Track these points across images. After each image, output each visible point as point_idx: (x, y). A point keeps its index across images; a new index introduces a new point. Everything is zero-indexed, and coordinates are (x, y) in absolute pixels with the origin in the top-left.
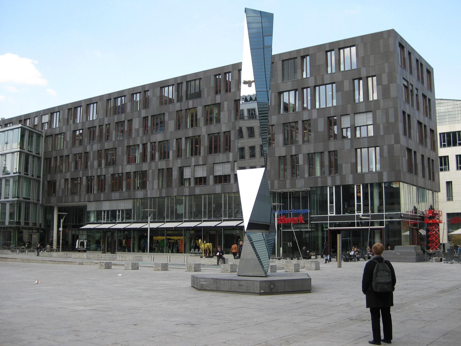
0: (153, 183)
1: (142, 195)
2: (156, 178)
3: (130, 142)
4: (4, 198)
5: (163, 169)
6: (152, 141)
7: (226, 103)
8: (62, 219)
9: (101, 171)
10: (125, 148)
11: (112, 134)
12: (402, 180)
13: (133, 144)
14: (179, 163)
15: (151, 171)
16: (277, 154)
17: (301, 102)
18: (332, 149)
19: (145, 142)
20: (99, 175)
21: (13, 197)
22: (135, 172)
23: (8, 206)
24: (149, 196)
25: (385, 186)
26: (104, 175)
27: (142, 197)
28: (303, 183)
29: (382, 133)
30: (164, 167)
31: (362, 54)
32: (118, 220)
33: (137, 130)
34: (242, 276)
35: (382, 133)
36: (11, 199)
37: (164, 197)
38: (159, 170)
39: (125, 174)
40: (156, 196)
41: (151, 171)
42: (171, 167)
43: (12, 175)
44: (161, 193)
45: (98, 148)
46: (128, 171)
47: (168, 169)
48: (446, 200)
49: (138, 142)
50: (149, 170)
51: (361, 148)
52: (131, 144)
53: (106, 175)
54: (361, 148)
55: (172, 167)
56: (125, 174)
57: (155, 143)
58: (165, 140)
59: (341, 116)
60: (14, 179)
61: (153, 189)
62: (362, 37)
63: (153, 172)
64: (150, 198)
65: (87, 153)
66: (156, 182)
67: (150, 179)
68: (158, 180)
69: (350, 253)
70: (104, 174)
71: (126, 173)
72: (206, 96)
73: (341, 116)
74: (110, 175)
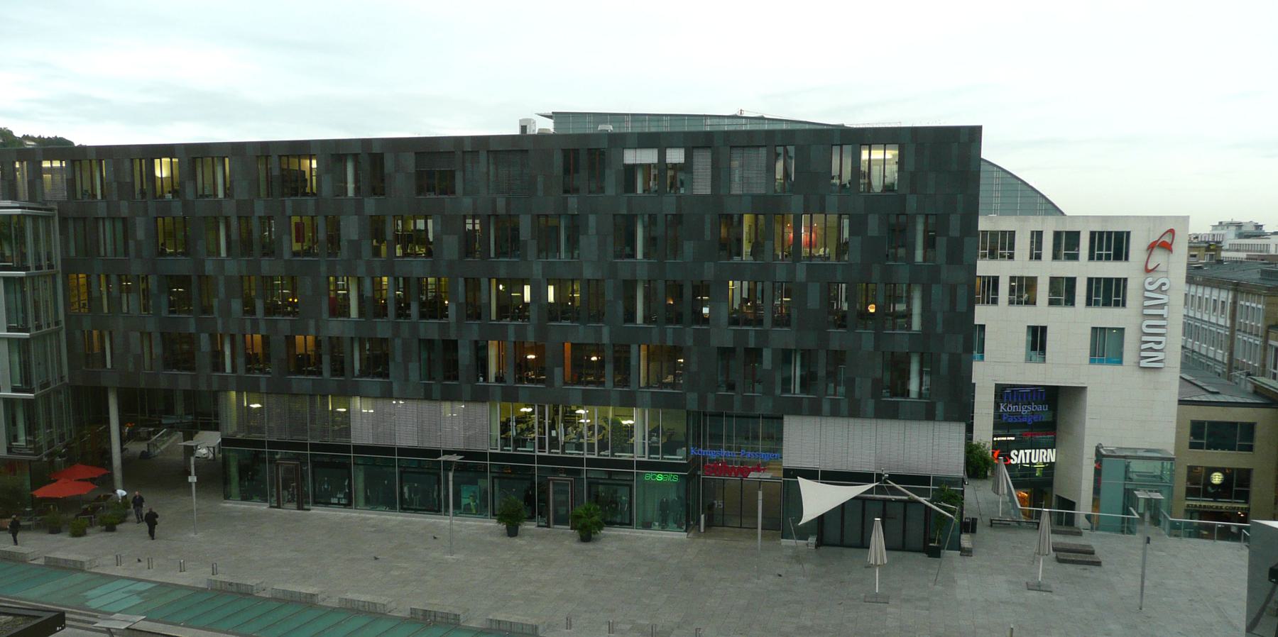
0: (406, 369)
7: (592, 219)
14: (474, 330)
15: (398, 342)
16: (715, 342)
18: (835, 345)
25: (804, 399)
28: (770, 405)
29: (939, 329)
30: (436, 337)
31: (910, 165)
33: (355, 246)
35: (939, 329)
41: (398, 342)
42: (453, 337)
48: (1088, 362)
53: (271, 338)
55: (456, 338)
59: (693, 147)
62: (915, 131)
65: (203, 278)
66: (414, 367)
67: (399, 358)
69: (1012, 461)
72: (540, 193)
73: (693, 147)
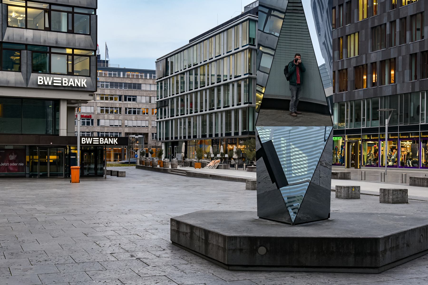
1: (391, 91)
2: (408, 67)
3: (375, 22)
4: (237, 104)
5: (416, 54)
6: (402, 16)
8: (387, 118)
9: (343, 65)
10: (369, 30)
11: (354, 12)
12: (95, 136)
13: (379, 24)
15: (400, 58)
17: (57, 117)
19: (392, 19)
20: (340, 69)
21: (245, 104)
22: (381, 62)
23: (240, 112)
24: (398, 92)
26: (346, 69)
27: (390, 94)
30: (418, 51)
32: (363, 126)
34: (372, 195)
36: (243, 105)
37: (418, 92)
38: (411, 55)
39: (369, 65)
40: (407, 92)
41: (400, 58)
43: (243, 77)
44: (413, 87)
45: (338, 35)
46: (373, 60)
47: (422, 53)
49: (384, 19)
50: (398, 57)
51: (47, 134)
52: (376, 24)
54: (47, 134)
56: (369, 65)
57: (405, 18)
58: (418, 12)
60: (245, 82)
61: (403, 82)
63: (404, 59)
64: (401, 95)
68: (410, 69)
70: (345, 68)
71: (371, 63)
74: (353, 68)
